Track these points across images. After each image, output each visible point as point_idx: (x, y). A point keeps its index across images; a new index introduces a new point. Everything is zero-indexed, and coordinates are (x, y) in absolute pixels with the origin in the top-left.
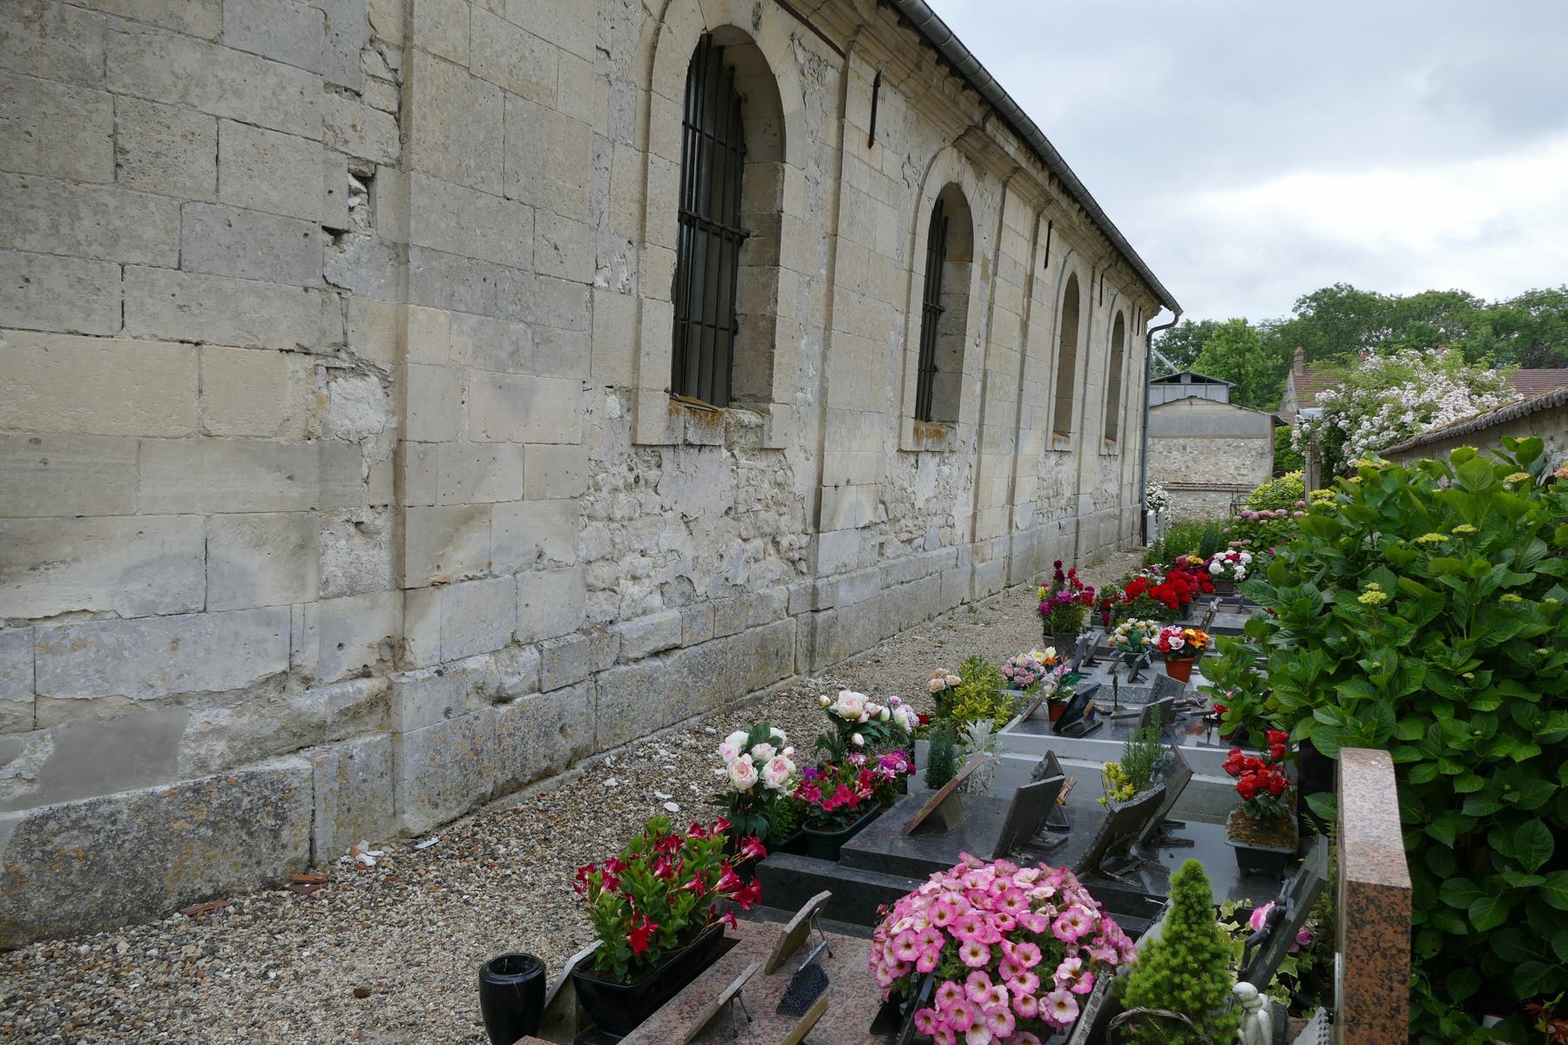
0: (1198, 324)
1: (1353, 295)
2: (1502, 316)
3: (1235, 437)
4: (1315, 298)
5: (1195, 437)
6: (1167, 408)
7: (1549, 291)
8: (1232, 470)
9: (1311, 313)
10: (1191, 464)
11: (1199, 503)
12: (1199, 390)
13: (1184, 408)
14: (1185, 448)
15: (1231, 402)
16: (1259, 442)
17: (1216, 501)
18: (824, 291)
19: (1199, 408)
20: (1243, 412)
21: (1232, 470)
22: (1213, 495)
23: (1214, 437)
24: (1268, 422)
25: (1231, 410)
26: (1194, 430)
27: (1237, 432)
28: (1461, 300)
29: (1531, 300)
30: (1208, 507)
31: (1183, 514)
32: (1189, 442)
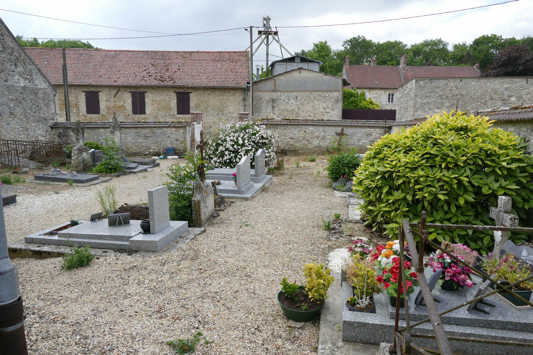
0: (307, 51)
1: (364, 40)
2: (417, 49)
3: (324, 91)
4: (350, 41)
5: (302, 91)
6: (288, 75)
7: (432, 40)
8: (322, 110)
9: (348, 47)
10: (300, 106)
11: (302, 134)
12: (305, 65)
13: (296, 74)
14: (297, 98)
15: (320, 72)
16: (335, 94)
17: (312, 133)
18: (328, 127)
19: (304, 74)
20: (327, 77)
21: (322, 110)
22: (311, 128)
23: (312, 91)
24: (341, 82)
25: (321, 75)
26: (302, 88)
27: (324, 88)
28: (399, 44)
29: (426, 44)
30: (308, 136)
31: (292, 142)
32: (300, 94)
